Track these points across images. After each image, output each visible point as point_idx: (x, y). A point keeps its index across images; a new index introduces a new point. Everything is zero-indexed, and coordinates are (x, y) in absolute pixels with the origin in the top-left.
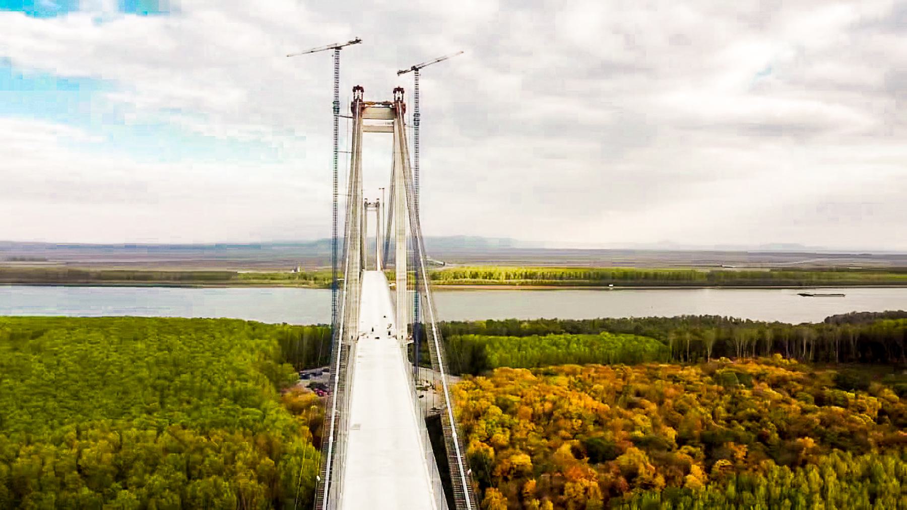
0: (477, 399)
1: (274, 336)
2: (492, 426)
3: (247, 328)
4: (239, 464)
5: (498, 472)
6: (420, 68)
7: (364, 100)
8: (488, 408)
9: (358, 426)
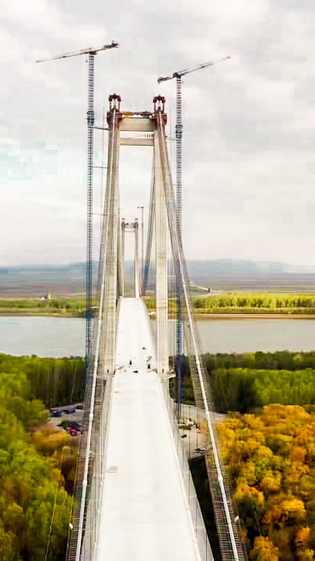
0: (245, 439)
2: (262, 469)
7: (122, 110)
8: (258, 449)
9: (114, 469)
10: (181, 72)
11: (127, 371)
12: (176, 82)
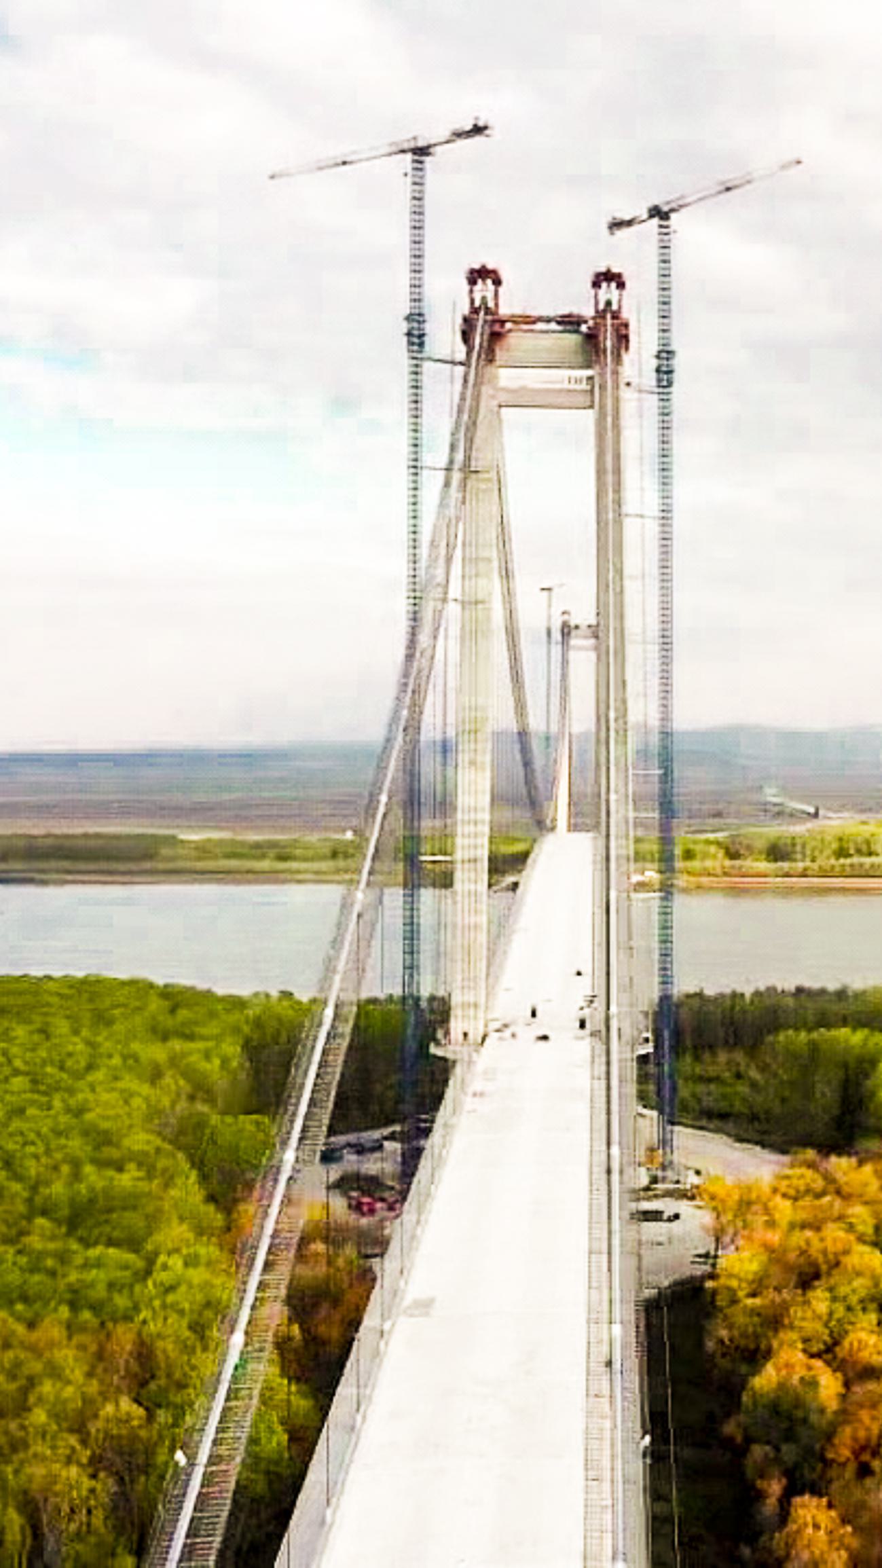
0: (816, 1226)
1: (236, 1030)
2: (849, 1309)
3: (155, 1005)
4: (39, 1416)
5: (842, 1450)
6: (673, 210)
7: (504, 311)
8: (846, 1252)
9: (424, 1306)
10: (668, 203)
11: (519, 1034)
12: (656, 230)
